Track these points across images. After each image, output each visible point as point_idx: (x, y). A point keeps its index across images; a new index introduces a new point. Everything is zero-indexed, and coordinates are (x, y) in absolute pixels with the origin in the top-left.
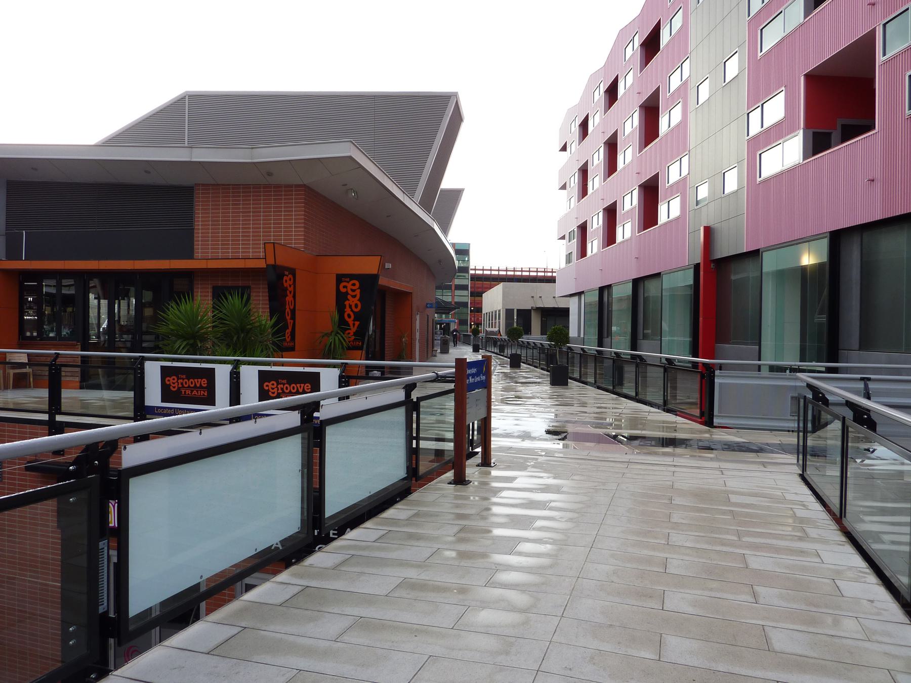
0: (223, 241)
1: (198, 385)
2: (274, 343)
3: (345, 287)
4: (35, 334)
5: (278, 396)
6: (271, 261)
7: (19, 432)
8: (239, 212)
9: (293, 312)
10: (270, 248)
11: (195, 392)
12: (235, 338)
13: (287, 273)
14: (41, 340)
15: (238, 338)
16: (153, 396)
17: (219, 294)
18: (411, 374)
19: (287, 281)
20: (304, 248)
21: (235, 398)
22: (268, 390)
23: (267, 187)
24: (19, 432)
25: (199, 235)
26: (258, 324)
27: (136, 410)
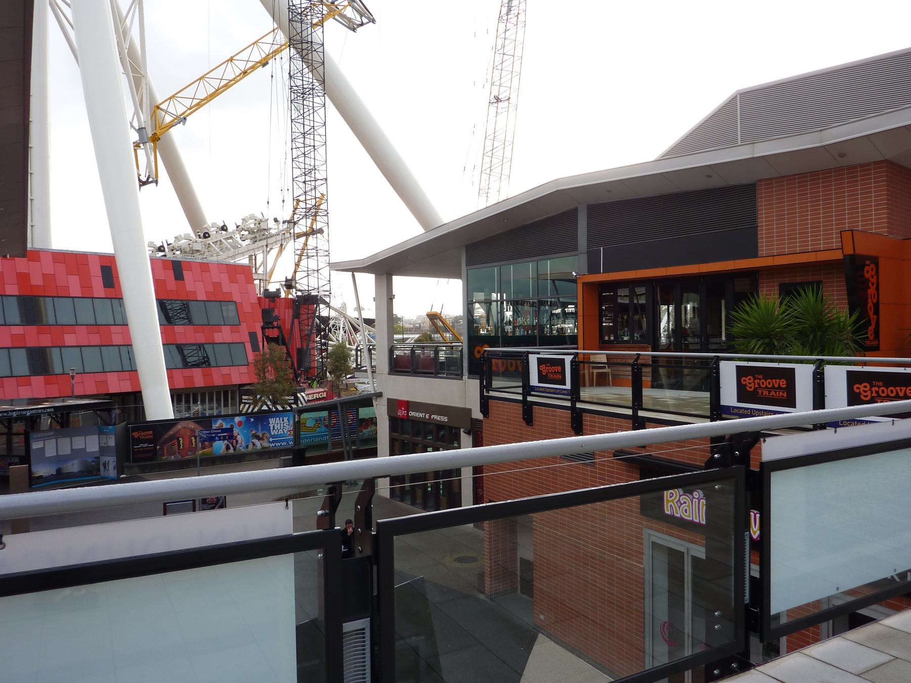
0: (787, 236)
1: (776, 386)
2: (855, 342)
3: (858, 388)
4: (612, 338)
5: (872, 401)
6: (849, 251)
7: (608, 424)
8: (807, 203)
9: (877, 306)
10: (847, 236)
11: (773, 393)
12: (811, 337)
13: (868, 262)
14: (618, 344)
15: (815, 337)
16: (729, 396)
17: (788, 291)
19: (869, 272)
20: (888, 232)
21: (819, 401)
22: (860, 393)
23: (839, 170)
24: (608, 424)
25: (763, 233)
26: (836, 321)
27: (712, 409)
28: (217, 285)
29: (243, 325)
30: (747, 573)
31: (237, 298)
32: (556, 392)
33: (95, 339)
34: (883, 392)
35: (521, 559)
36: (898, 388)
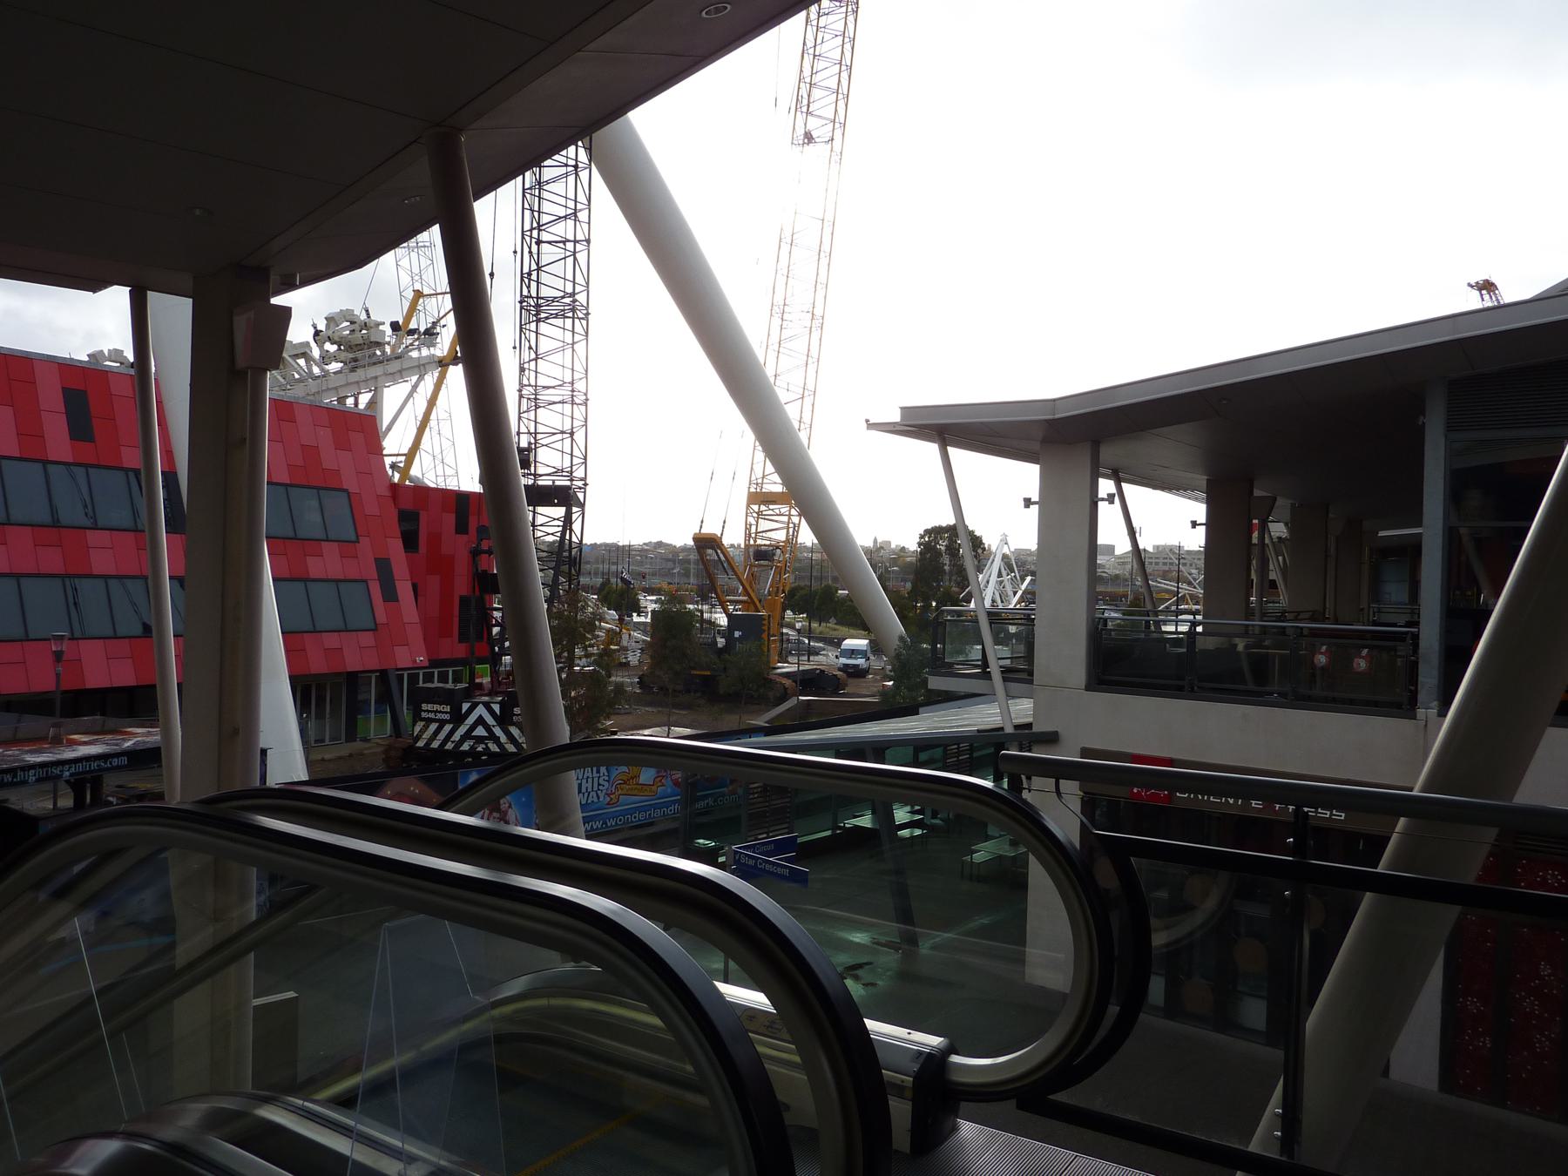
28: (311, 452)
29: (365, 541)
31: (350, 484)
33: (52, 560)
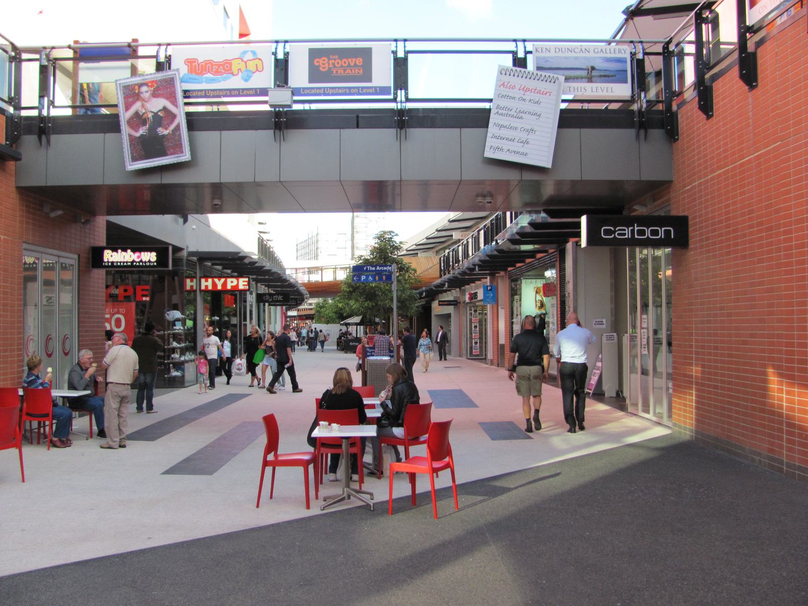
1: (352, 64)
3: (318, 62)
11: (348, 71)
18: (631, 314)
22: (319, 66)
30: (130, 80)
32: (360, 91)
34: (338, 63)
35: (477, 293)
36: (350, 60)
